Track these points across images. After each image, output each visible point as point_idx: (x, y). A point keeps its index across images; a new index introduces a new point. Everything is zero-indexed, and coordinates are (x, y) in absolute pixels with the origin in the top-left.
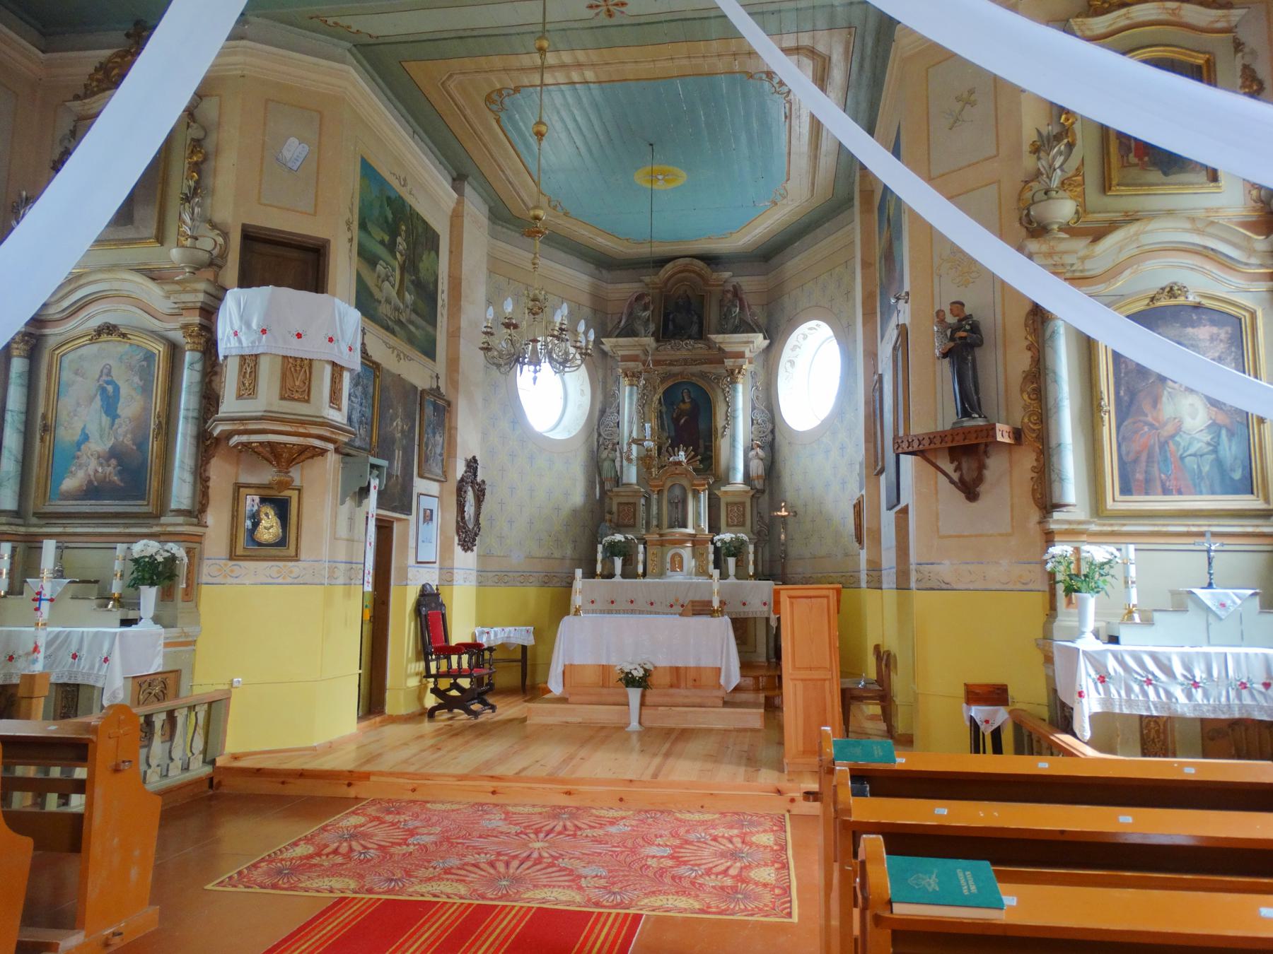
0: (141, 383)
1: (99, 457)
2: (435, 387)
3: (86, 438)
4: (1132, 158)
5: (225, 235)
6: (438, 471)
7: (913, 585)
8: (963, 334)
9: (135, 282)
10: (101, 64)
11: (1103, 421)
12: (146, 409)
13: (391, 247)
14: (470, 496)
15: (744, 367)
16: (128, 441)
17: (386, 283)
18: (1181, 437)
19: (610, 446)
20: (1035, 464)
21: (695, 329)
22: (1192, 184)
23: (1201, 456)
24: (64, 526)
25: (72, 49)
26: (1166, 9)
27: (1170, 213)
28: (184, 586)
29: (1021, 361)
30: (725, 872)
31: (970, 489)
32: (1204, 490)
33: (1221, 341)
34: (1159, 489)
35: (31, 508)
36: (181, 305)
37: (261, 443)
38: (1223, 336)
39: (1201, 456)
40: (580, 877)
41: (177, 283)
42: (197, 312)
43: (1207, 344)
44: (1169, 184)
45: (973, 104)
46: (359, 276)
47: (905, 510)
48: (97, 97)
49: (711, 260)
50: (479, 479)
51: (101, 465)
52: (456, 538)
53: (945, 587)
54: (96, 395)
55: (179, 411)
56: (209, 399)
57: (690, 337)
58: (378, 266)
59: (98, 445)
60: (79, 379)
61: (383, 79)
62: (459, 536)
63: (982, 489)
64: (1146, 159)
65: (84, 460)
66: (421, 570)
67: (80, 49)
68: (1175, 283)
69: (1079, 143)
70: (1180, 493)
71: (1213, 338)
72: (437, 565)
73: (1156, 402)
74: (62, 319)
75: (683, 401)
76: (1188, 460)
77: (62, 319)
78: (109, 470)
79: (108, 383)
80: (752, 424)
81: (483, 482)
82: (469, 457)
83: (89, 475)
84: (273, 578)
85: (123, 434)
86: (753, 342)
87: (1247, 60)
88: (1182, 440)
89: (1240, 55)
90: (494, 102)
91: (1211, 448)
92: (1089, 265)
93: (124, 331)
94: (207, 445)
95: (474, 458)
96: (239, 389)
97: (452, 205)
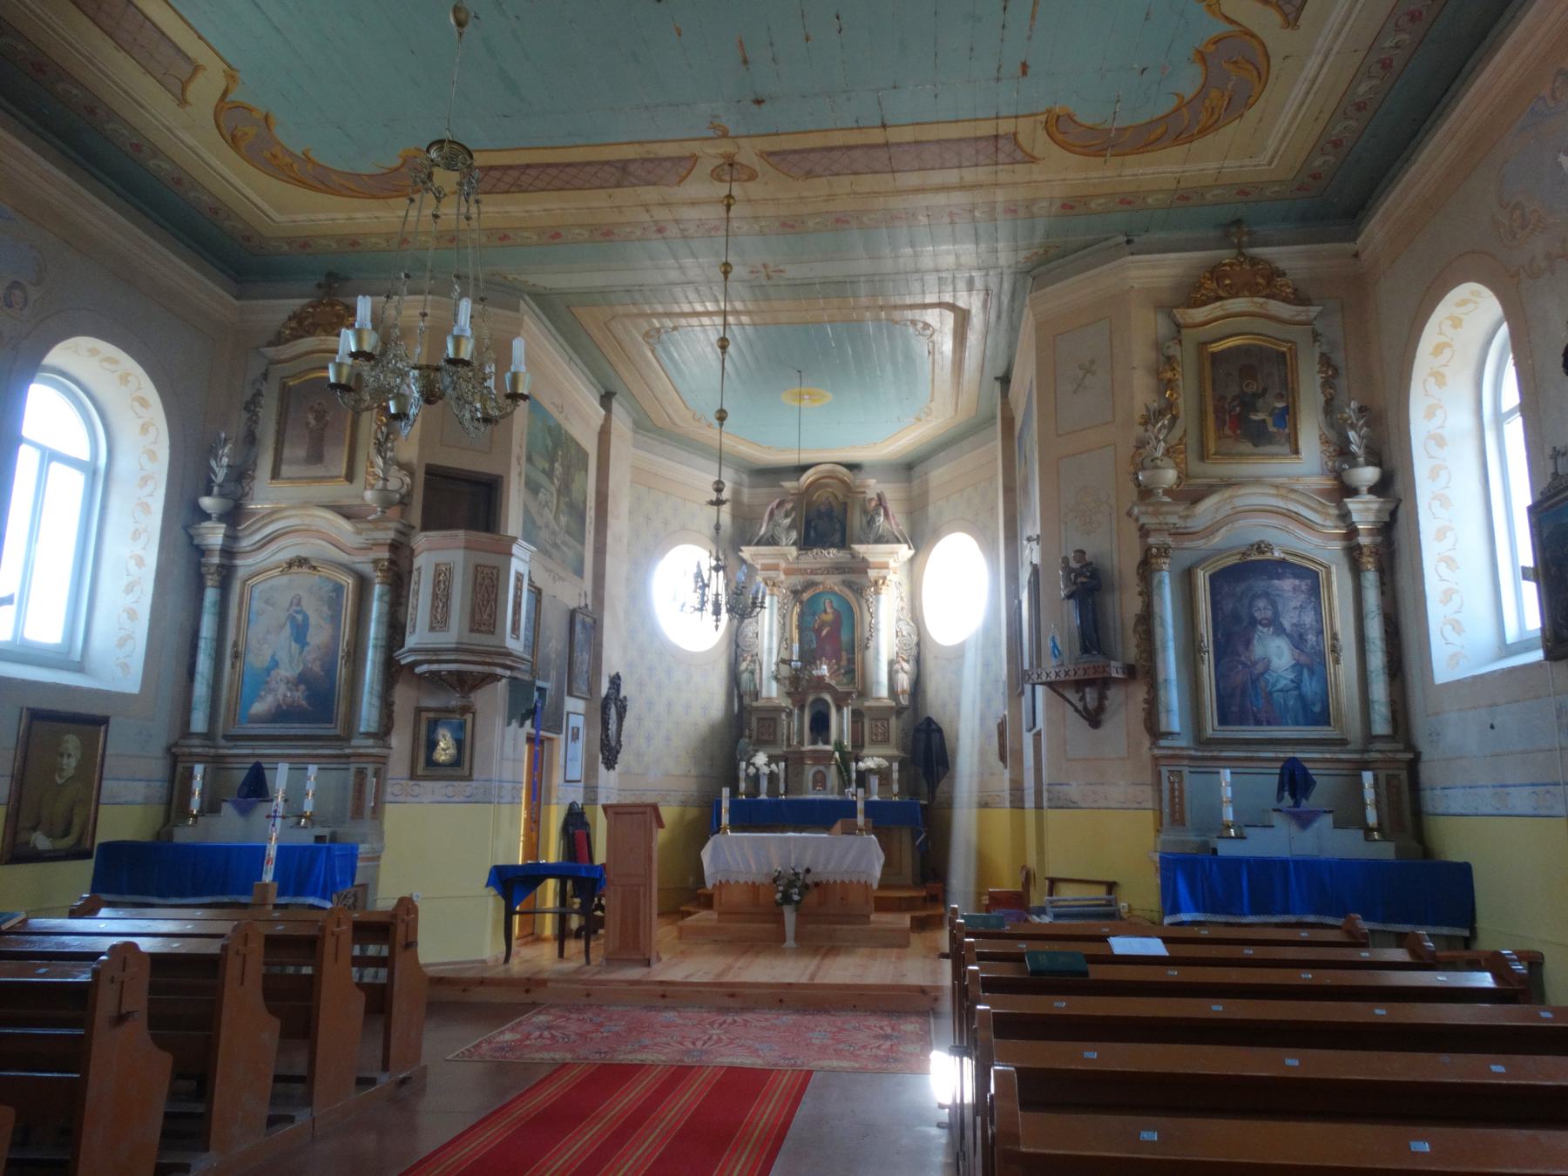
0: (330, 613)
1: (288, 683)
2: (583, 604)
3: (275, 664)
4: (1227, 431)
5: (412, 475)
6: (584, 688)
7: (1045, 804)
8: (1084, 580)
9: (324, 518)
10: (295, 313)
11: (1203, 661)
12: (335, 638)
13: (549, 474)
14: (613, 712)
15: (888, 578)
16: (316, 668)
17: (546, 509)
18: (1270, 675)
19: (749, 658)
20: (1146, 696)
21: (837, 537)
22: (1277, 455)
23: (1287, 691)
24: (253, 748)
25: (263, 298)
26: (1256, 303)
27: (1257, 481)
28: (372, 804)
29: (1133, 605)
30: (879, 1047)
31: (1094, 718)
32: (1289, 721)
33: (1303, 592)
34: (1252, 721)
35: (220, 731)
36: (371, 542)
37: (450, 672)
38: (1304, 587)
39: (1287, 691)
40: (757, 1050)
41: (370, 522)
42: (387, 548)
43: (1291, 594)
44: (1259, 455)
45: (1094, 374)
46: (525, 505)
47: (1038, 734)
48: (291, 344)
49: (853, 467)
50: (623, 694)
51: (290, 690)
52: (600, 756)
53: (1069, 805)
54: (285, 624)
55: (368, 640)
56: (396, 630)
57: (833, 546)
58: (540, 494)
59: (286, 671)
60: (270, 608)
61: (567, 340)
62: (603, 754)
63: (1104, 717)
64: (1239, 432)
65: (273, 685)
66: (569, 789)
67: (274, 298)
68: (1262, 541)
69: (1182, 415)
70: (1269, 723)
71: (1295, 589)
72: (582, 784)
73: (1248, 643)
74: (254, 551)
75: (825, 612)
76: (1275, 695)
77: (254, 551)
78: (298, 694)
79: (297, 612)
80: (897, 636)
81: (625, 698)
82: (613, 673)
83: (278, 700)
84: (396, 796)
85: (312, 658)
86: (897, 553)
87: (1325, 349)
88: (1270, 677)
89: (1318, 344)
90: (652, 337)
91: (1295, 685)
92: (1190, 523)
93: (314, 564)
94: (392, 671)
95: (617, 674)
96: (431, 622)
97: (600, 422)
